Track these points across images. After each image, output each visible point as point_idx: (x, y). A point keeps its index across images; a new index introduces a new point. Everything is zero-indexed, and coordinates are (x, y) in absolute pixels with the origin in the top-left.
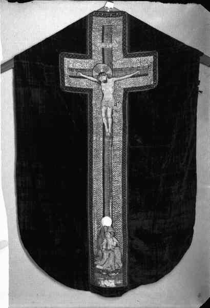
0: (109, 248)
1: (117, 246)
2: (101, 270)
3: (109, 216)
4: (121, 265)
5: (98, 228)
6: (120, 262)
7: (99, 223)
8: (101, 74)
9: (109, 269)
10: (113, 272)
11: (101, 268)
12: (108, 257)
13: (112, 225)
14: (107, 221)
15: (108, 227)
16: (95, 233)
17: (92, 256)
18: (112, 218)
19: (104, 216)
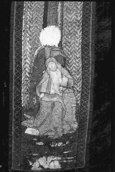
0: (52, 92)
1: (68, 87)
2: (34, 136)
3: (56, 24)
4: (76, 126)
5: (33, 49)
6: (75, 120)
7: (35, 41)
8: (29, 28)
9: (51, 135)
10: (57, 140)
11: (36, 132)
12: (49, 110)
13: (61, 42)
14: (50, 36)
15: (52, 48)
16: (27, 63)
17: (17, 109)
18: (61, 29)
19: (45, 26)
